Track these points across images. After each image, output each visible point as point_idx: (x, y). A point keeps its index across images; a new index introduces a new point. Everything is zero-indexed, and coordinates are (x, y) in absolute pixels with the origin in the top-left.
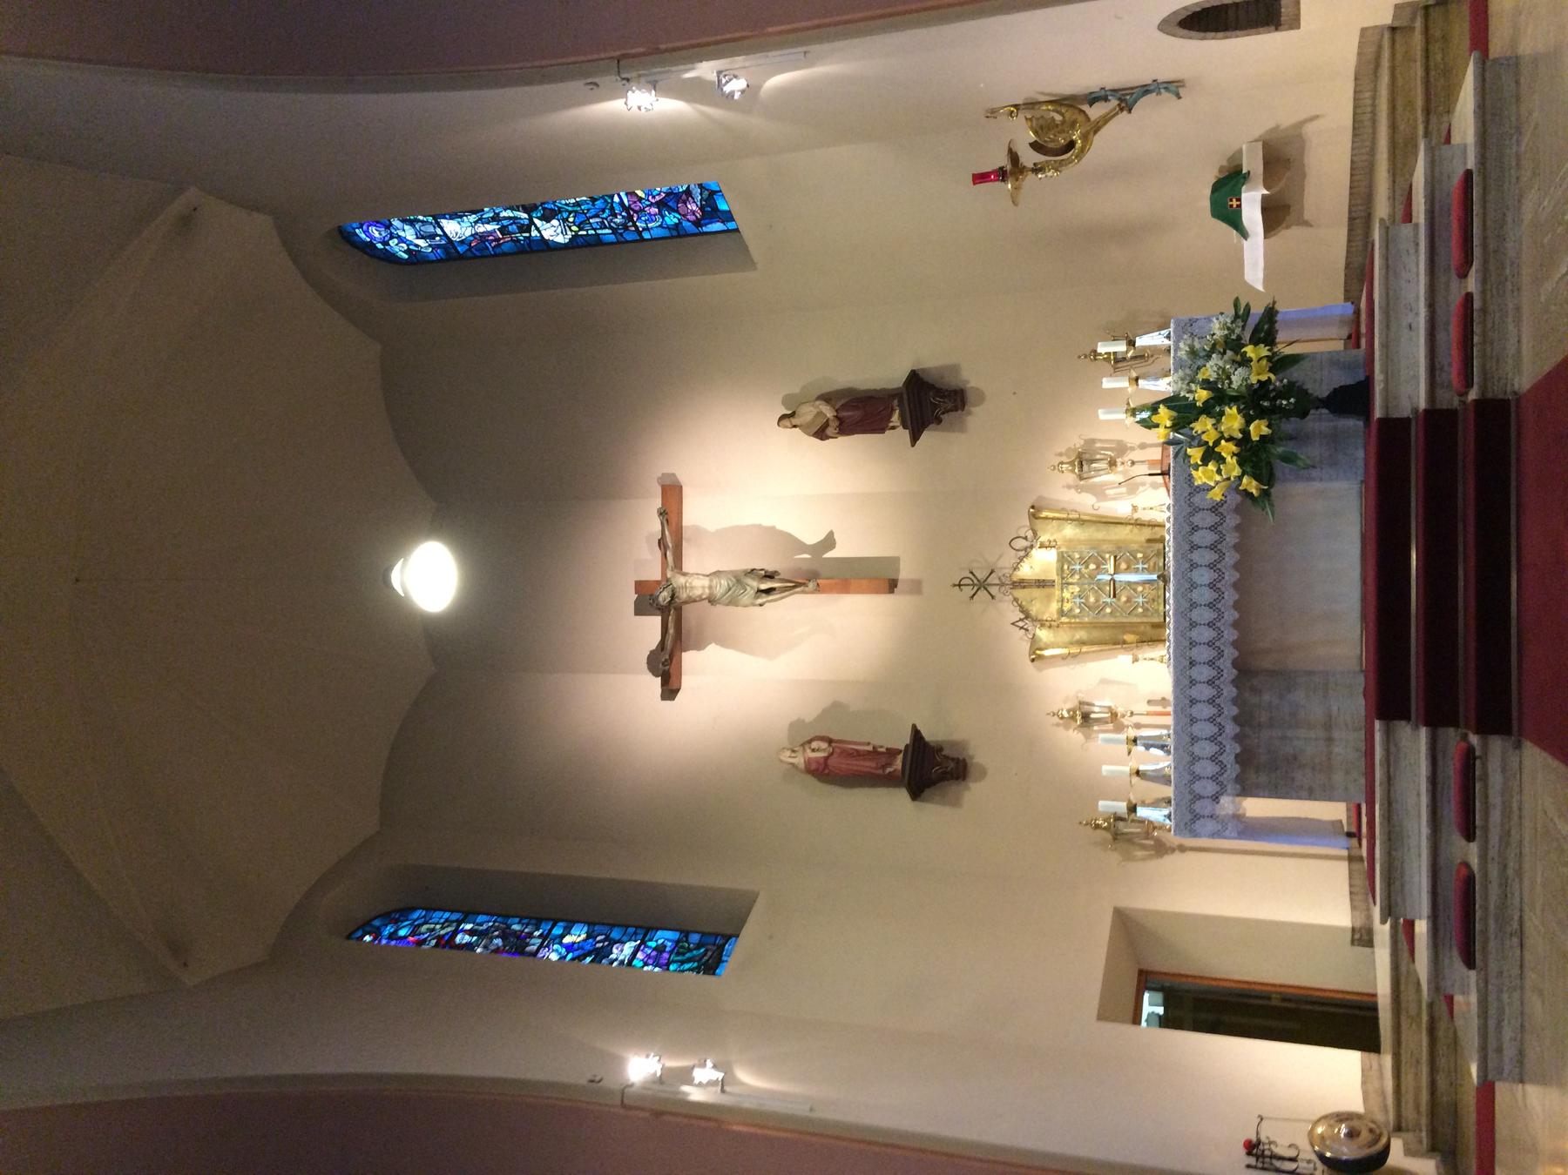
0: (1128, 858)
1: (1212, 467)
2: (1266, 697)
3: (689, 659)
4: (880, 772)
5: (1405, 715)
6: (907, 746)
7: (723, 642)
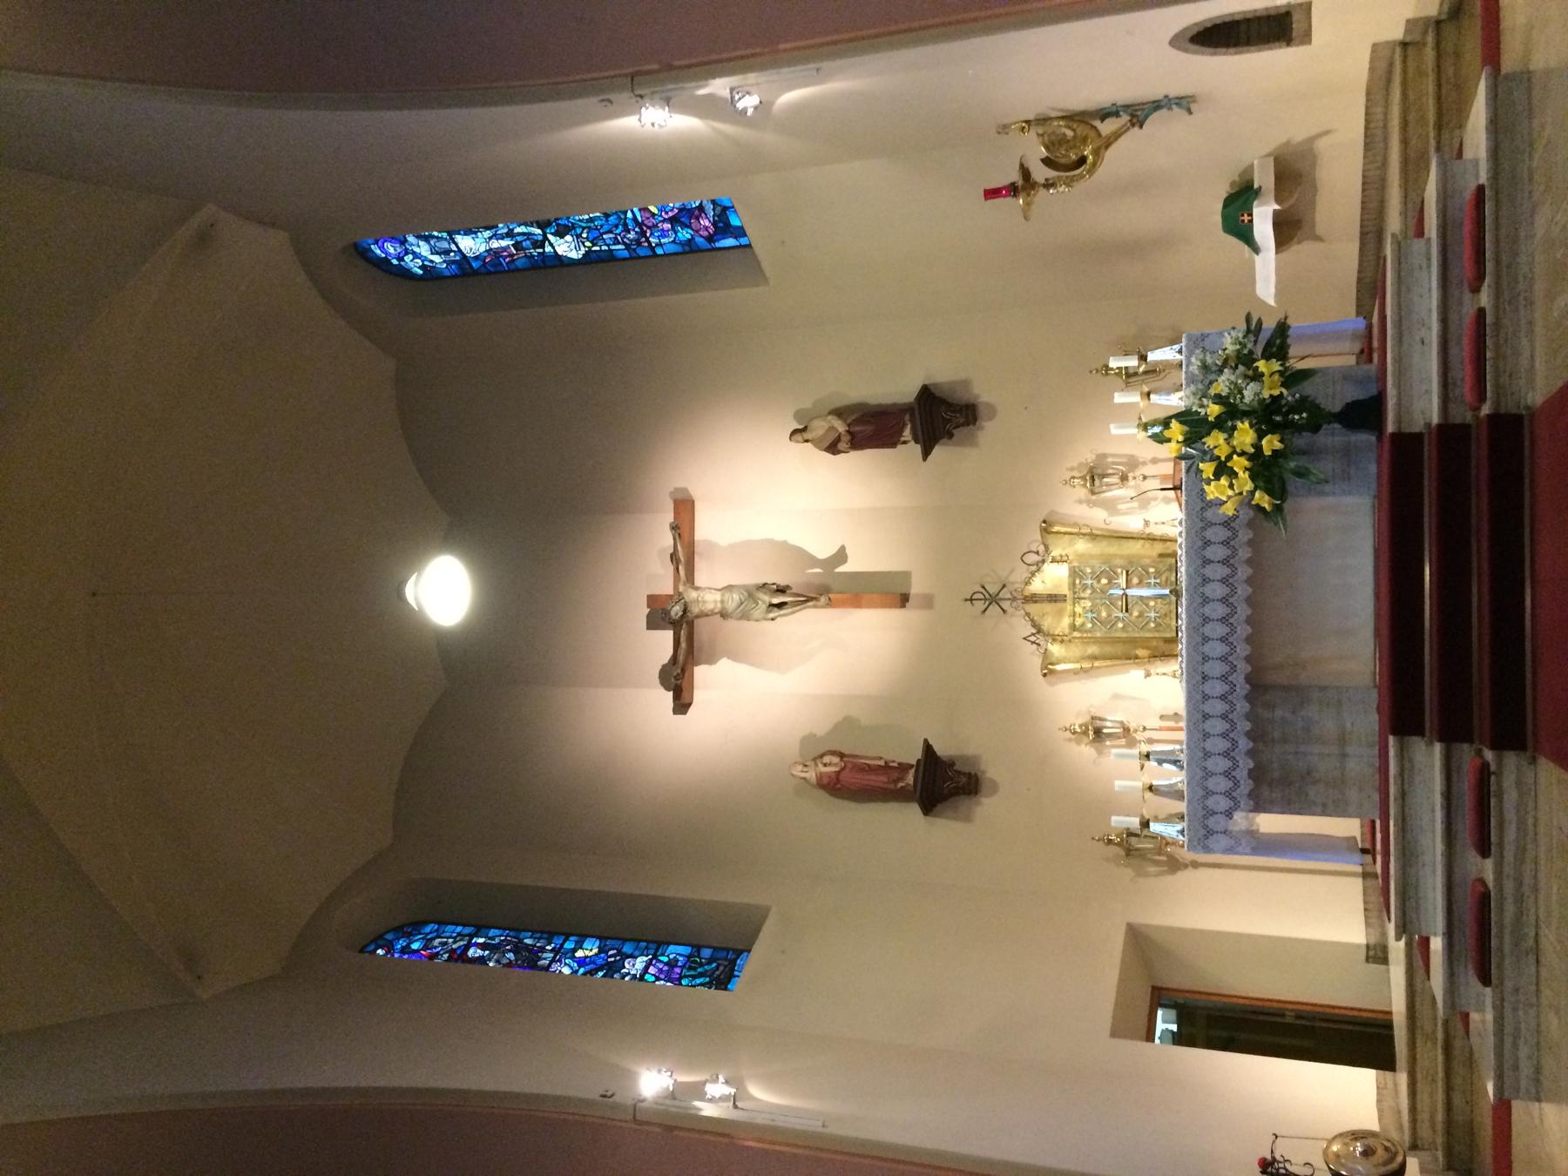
1: (1224, 481)
2: (1279, 713)
4: (892, 786)
5: (1420, 732)
6: (919, 761)
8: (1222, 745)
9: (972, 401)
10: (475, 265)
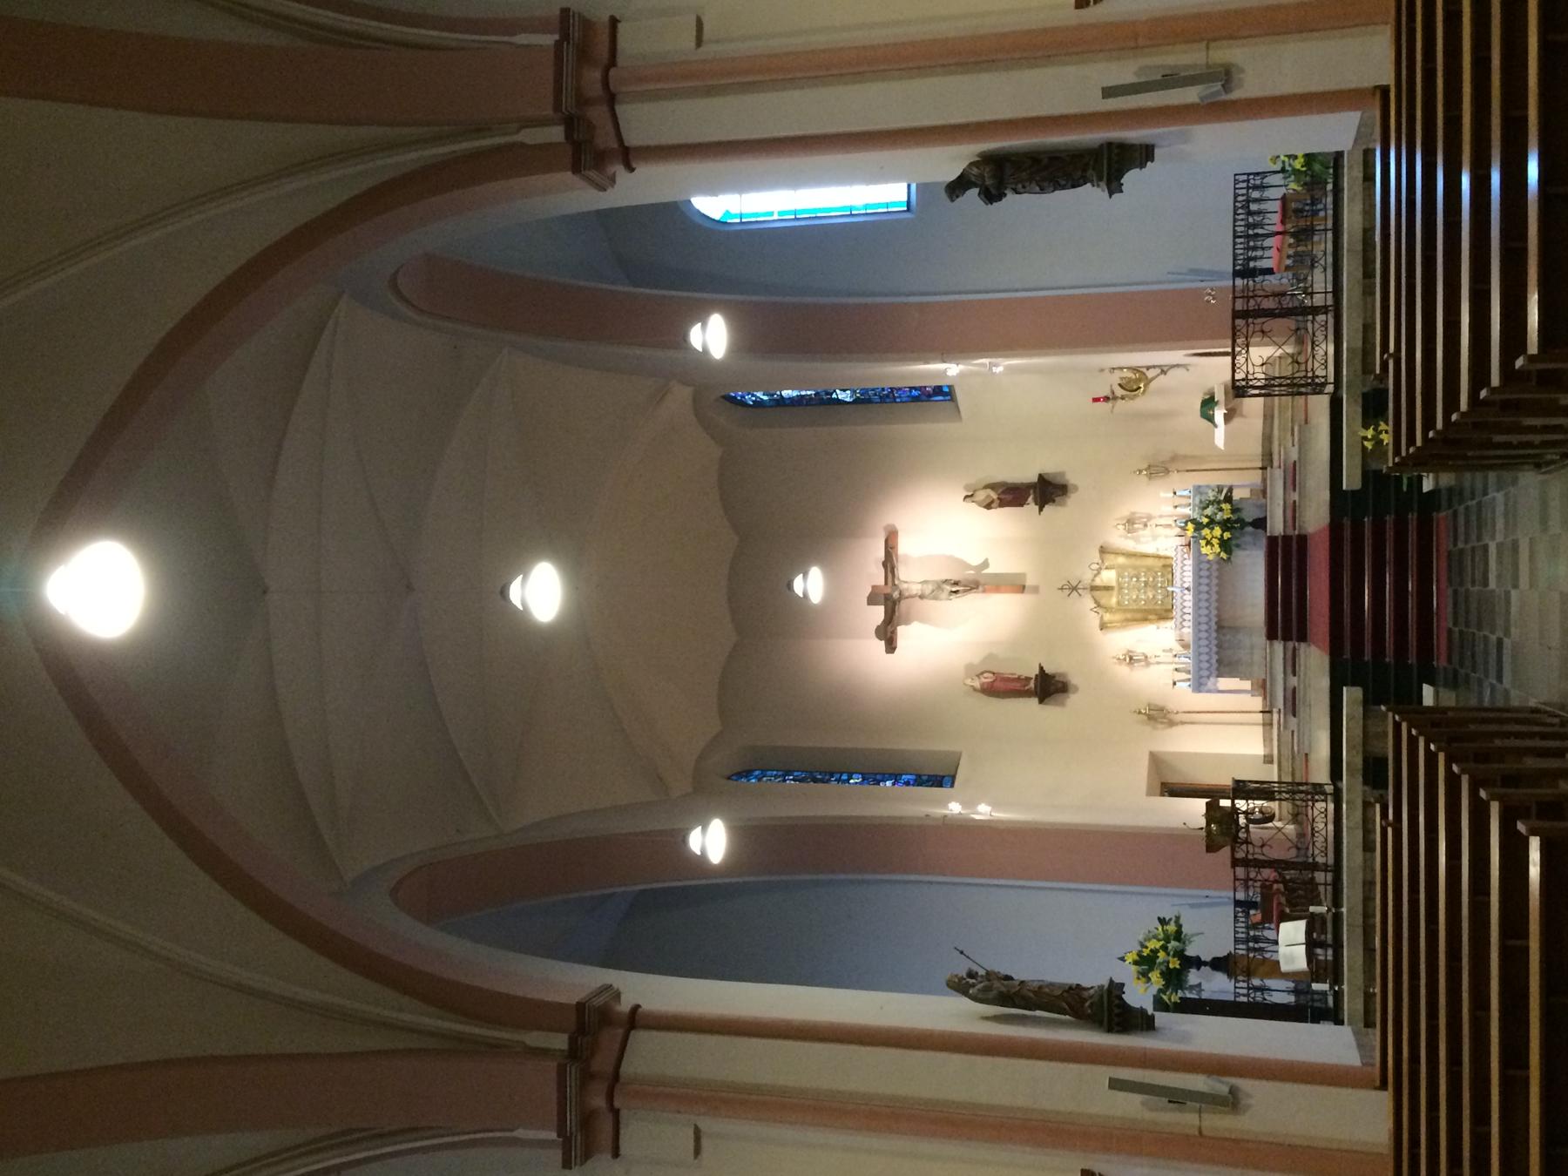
0: (1155, 728)
1: (1209, 547)
2: (1228, 637)
3: (902, 631)
4: (1022, 689)
5: (1276, 638)
6: (1037, 675)
7: (922, 620)
8: (1206, 642)
9: (1064, 483)
10: (787, 402)
